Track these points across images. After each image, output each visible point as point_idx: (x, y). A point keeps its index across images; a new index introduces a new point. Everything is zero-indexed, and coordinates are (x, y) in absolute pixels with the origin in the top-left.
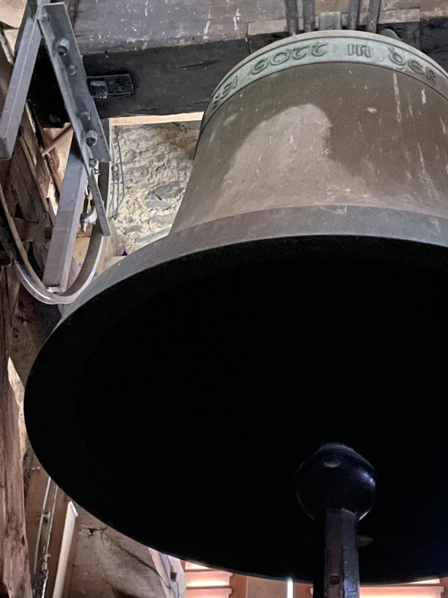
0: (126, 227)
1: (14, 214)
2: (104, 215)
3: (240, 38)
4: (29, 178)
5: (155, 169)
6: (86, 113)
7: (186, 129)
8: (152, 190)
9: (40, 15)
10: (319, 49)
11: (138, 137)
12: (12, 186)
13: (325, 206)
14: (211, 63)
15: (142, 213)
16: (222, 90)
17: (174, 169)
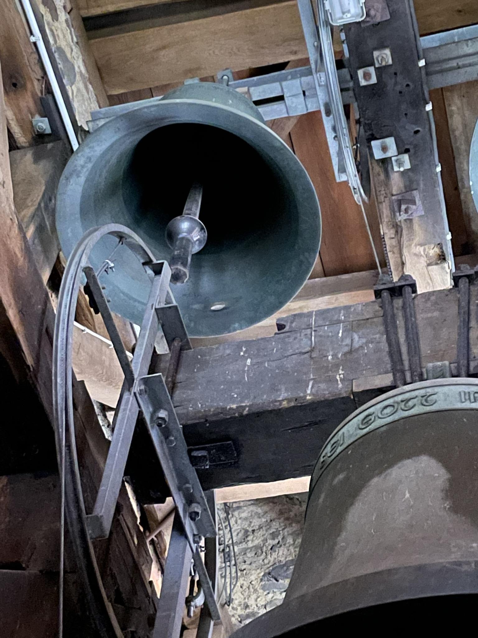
0: (242, 615)
1: (113, 600)
2: (212, 596)
3: (345, 395)
4: (130, 559)
5: (270, 547)
6: (188, 485)
7: (300, 502)
8: (267, 571)
9: (137, 387)
10: (429, 399)
11: (250, 515)
12: (111, 569)
13: (449, 563)
14: (316, 423)
15: (258, 597)
16: (329, 448)
17: (290, 546)
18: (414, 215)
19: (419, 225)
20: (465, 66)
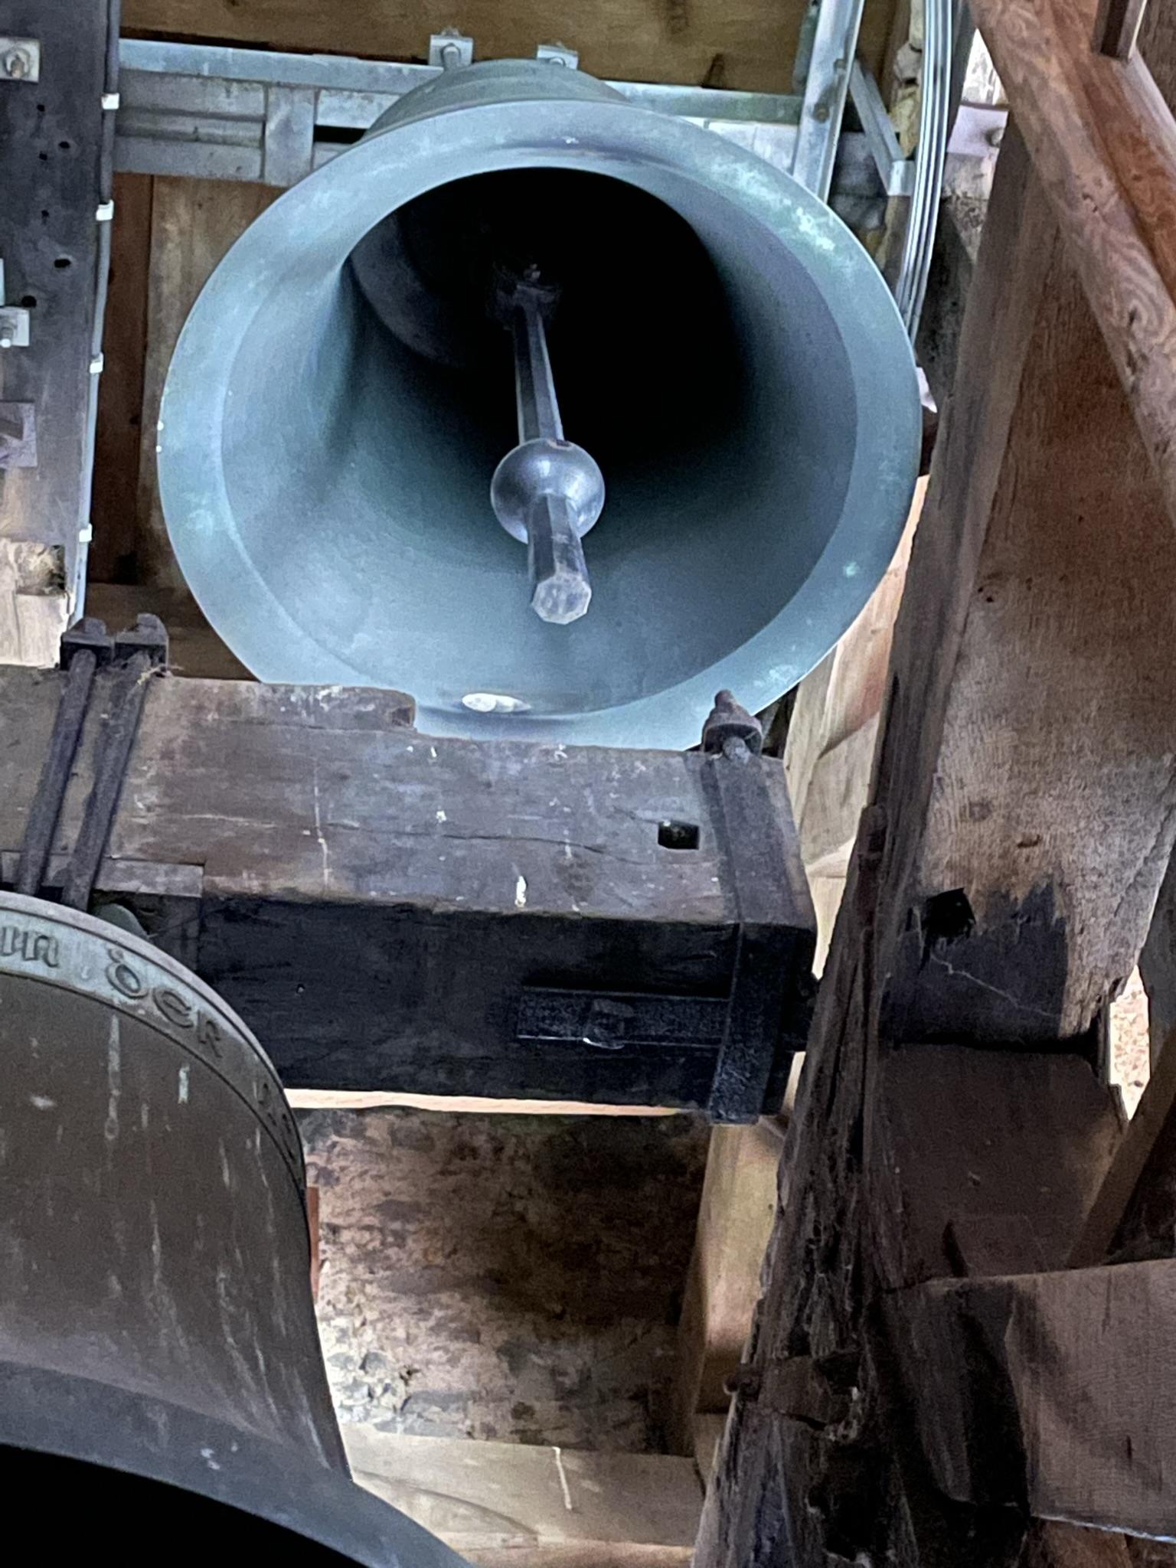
18: (11, 461)
19: (18, 491)
20: (211, 140)
